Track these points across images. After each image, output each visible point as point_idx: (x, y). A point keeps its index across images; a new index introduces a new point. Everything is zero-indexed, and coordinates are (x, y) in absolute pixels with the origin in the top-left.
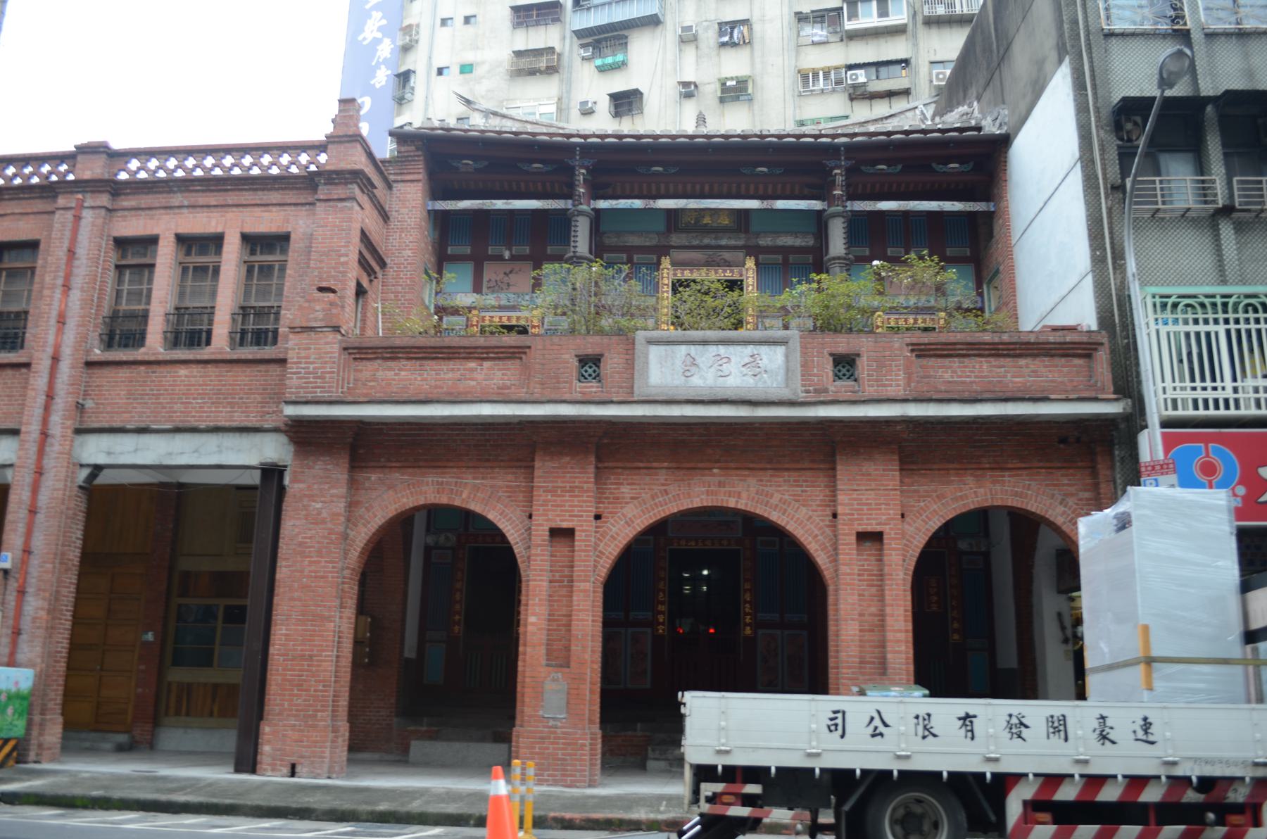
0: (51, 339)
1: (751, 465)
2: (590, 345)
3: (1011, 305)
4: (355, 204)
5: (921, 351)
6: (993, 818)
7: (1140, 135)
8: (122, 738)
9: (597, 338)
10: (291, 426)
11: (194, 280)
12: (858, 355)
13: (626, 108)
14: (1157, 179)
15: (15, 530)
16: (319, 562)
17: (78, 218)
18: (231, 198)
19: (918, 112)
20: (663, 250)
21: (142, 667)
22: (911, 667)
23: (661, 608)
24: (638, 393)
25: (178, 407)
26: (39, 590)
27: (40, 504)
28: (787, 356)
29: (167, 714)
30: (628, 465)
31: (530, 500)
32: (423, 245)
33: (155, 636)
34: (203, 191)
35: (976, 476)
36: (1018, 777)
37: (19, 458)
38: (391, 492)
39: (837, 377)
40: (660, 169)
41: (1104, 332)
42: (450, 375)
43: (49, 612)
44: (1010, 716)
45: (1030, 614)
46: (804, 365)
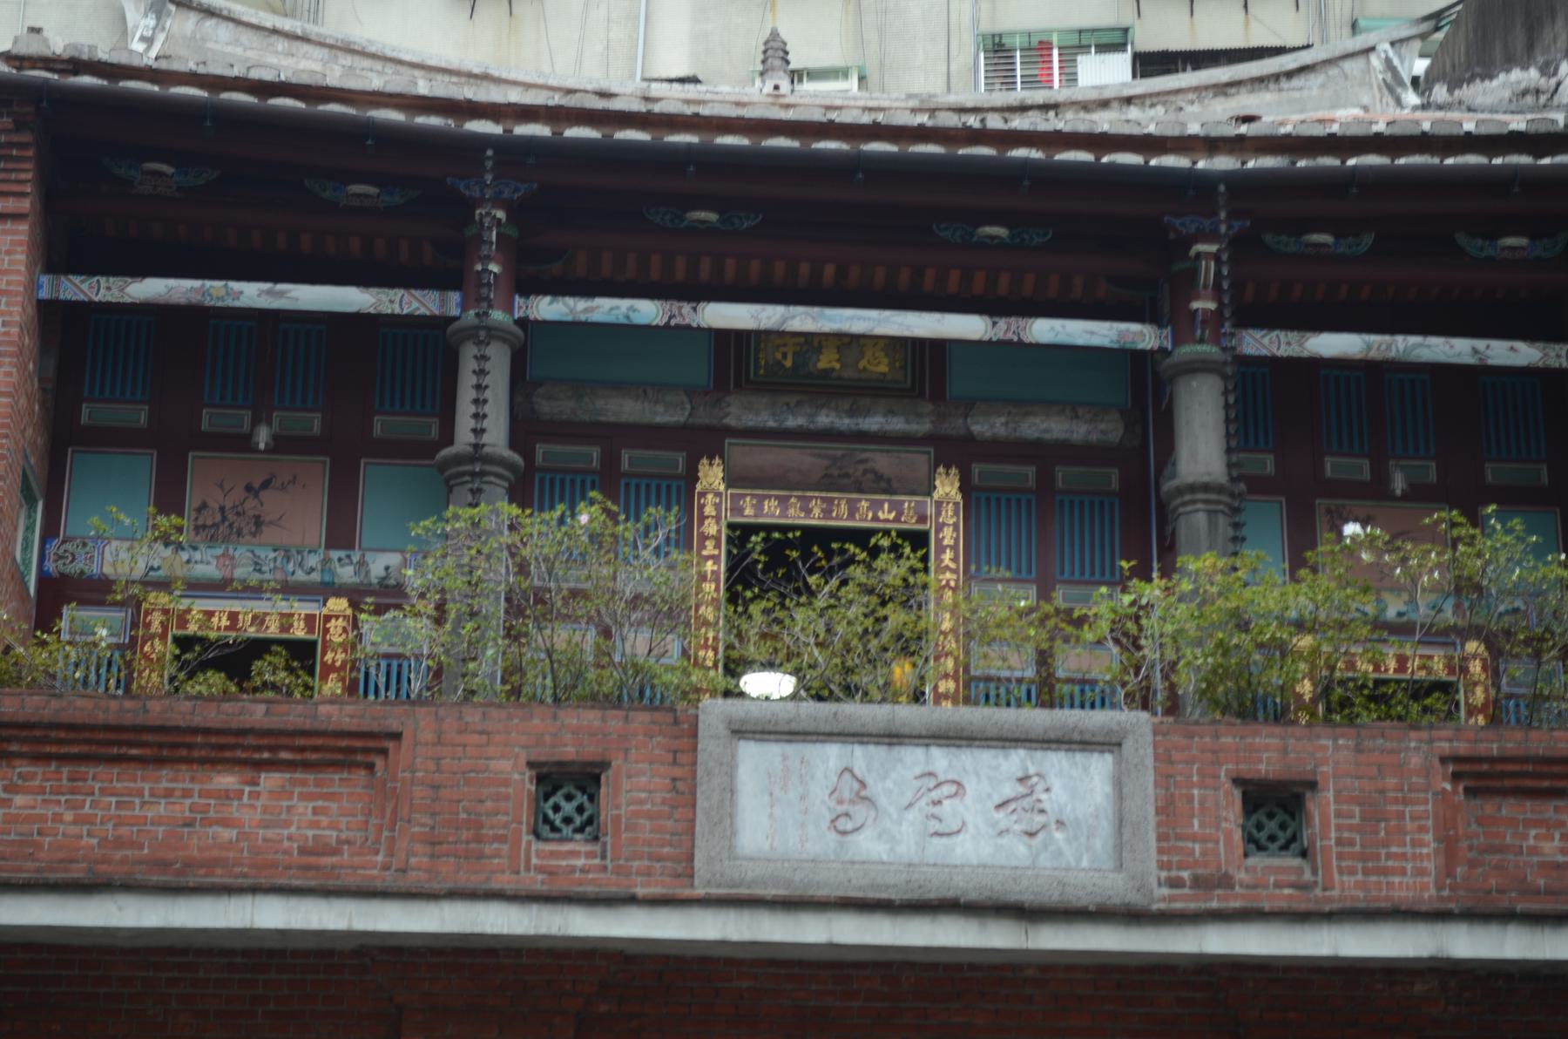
2: (572, 734)
9: (591, 717)
12: (1312, 785)
19: (1376, 61)
20: (704, 441)
24: (707, 875)
28: (1118, 784)
32: (23, 402)
39: (1254, 843)
40: (712, 217)
42: (162, 809)
46: (1166, 810)
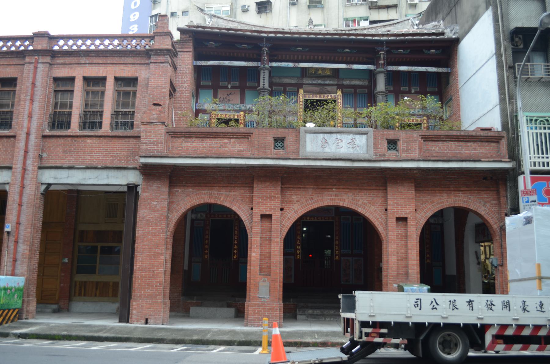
0: (25, 124)
1: (350, 187)
2: (280, 133)
3: (457, 115)
4: (168, 65)
5: (426, 138)
6: (480, 342)
7: (526, 46)
8: (55, 307)
10: (142, 167)
11: (92, 98)
12: (399, 140)
13: (263, 9)
14: (529, 64)
15: (12, 214)
16: (156, 229)
17: (36, 68)
18: (109, 60)
19: (410, 21)
20: (300, 86)
21: (63, 274)
22: (419, 276)
23: (298, 247)
25: (87, 157)
26: (25, 241)
27: (23, 202)
28: (367, 140)
29: (74, 295)
30: (295, 186)
31: (252, 202)
33: (69, 260)
34: (95, 56)
35: (447, 193)
36: (489, 326)
37: (12, 180)
38: (188, 197)
39: (389, 149)
40: (301, 49)
41: (504, 132)
42: (216, 145)
43: (30, 251)
44: (487, 301)
45: (463, 252)
